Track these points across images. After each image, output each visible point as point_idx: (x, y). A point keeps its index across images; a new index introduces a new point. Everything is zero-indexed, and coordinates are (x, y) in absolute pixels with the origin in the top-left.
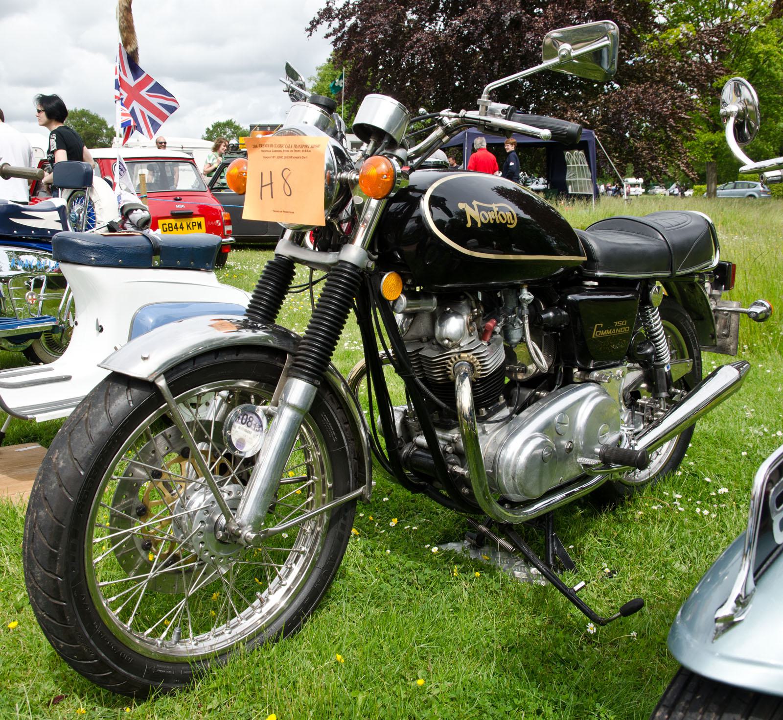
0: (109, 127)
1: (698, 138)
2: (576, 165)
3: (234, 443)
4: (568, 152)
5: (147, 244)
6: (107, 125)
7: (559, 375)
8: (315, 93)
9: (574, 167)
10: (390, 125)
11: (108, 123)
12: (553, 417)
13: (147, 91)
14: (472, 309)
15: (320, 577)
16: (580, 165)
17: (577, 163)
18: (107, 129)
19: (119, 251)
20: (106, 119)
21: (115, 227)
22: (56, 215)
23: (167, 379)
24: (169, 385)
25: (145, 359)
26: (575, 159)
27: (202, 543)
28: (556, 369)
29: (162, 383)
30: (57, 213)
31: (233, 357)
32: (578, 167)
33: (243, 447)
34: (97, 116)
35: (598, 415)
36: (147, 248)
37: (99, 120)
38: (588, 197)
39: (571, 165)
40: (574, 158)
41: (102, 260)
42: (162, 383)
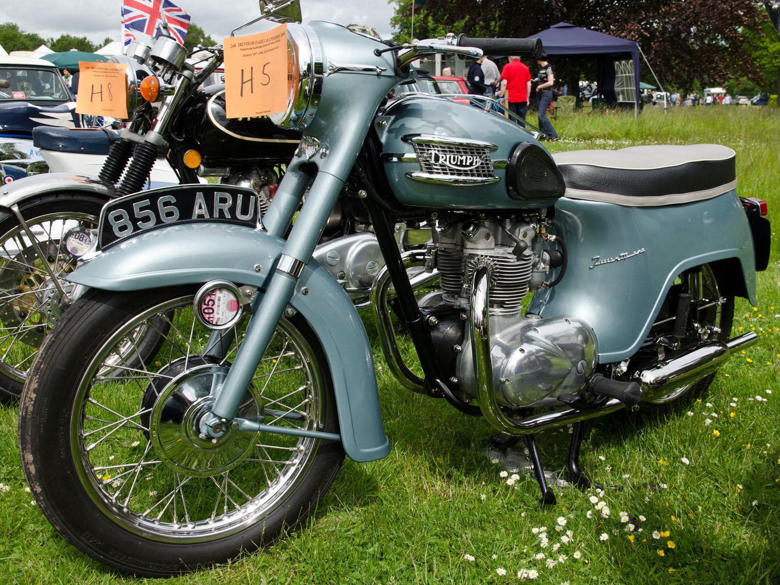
0: (206, 36)
1: (766, 48)
2: (624, 75)
3: (70, 250)
4: (617, 63)
5: (105, 136)
6: (203, 35)
7: (346, 227)
8: (402, 4)
9: (623, 77)
10: (170, 58)
11: (204, 33)
12: (326, 253)
13: (146, 20)
14: (260, 176)
15: (146, 347)
16: (627, 75)
17: (625, 73)
18: (203, 38)
19: (82, 141)
20: (203, 29)
21: (117, 126)
22: (69, 116)
23: (19, 208)
24: (22, 212)
25: (5, 194)
26: (625, 70)
27: (50, 311)
28: (345, 223)
29: (15, 209)
30: (70, 114)
31: (70, 198)
32: (626, 76)
33: (77, 252)
34: (195, 26)
35: (363, 254)
36: (105, 140)
37: (197, 30)
38: (631, 106)
39: (620, 75)
40: (622, 67)
41: (69, 147)
42: (15, 209)
